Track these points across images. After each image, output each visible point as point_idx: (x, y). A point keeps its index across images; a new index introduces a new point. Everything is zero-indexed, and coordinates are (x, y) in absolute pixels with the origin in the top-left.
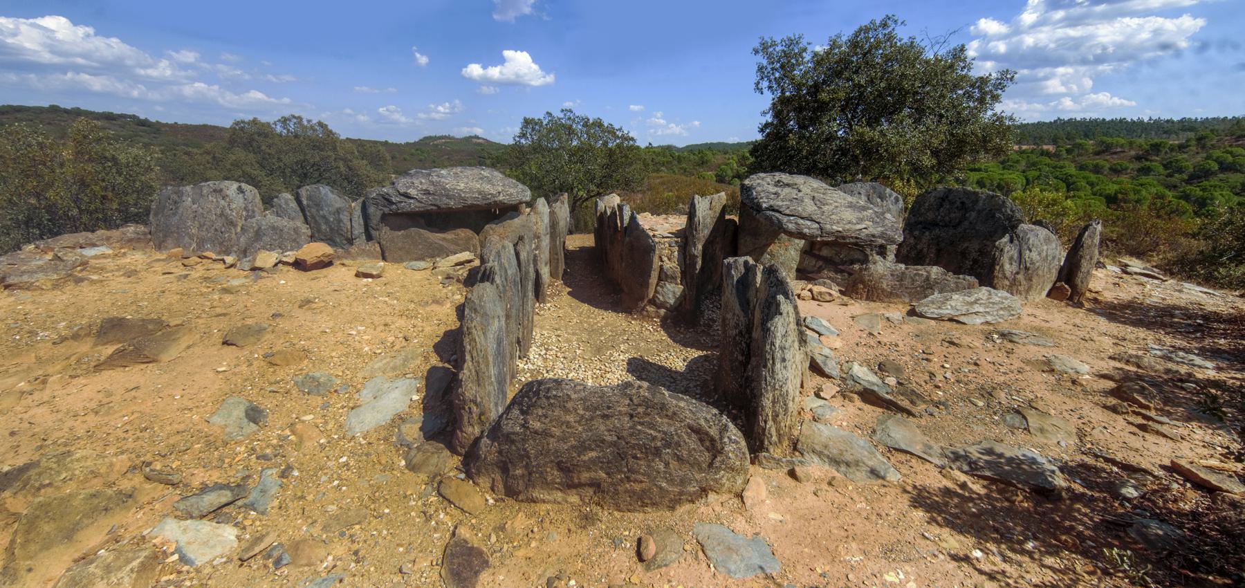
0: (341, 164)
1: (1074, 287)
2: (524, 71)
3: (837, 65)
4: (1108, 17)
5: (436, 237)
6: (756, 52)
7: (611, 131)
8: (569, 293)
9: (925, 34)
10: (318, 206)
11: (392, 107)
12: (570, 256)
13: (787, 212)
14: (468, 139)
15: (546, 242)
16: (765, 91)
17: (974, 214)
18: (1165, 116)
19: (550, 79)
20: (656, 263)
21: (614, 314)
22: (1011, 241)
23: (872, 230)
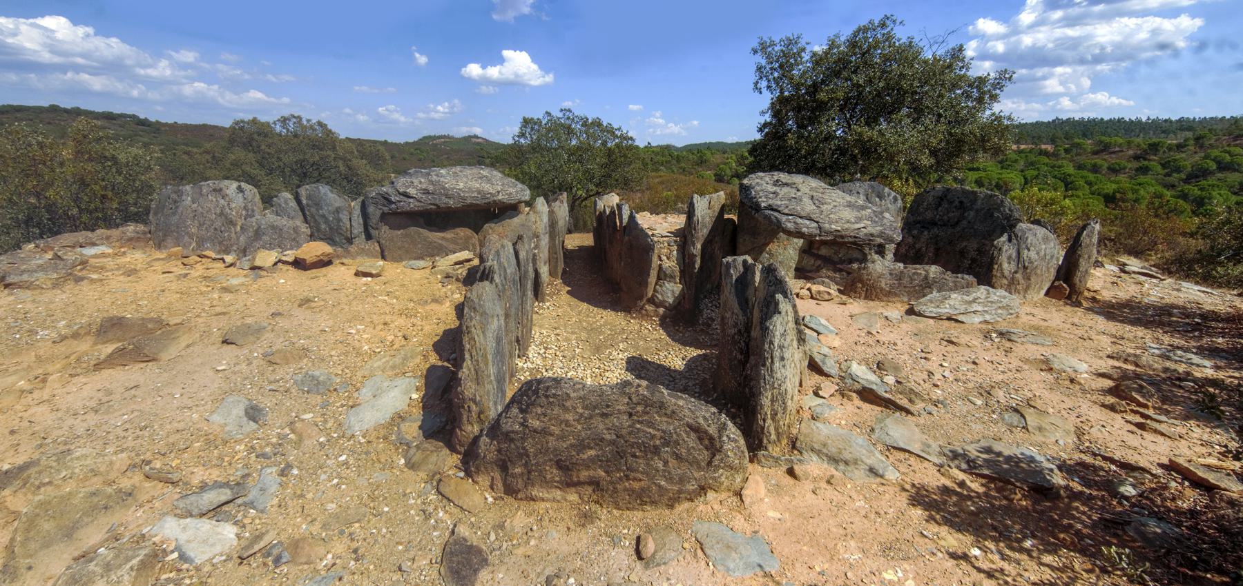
0: (340, 164)
1: (1072, 286)
2: (523, 70)
3: (836, 65)
4: (1106, 17)
5: (436, 236)
6: (755, 52)
7: (610, 131)
8: (568, 292)
9: (923, 34)
10: (317, 205)
11: (392, 107)
12: (569, 255)
13: (786, 211)
14: (467, 139)
15: (545, 241)
16: (764, 90)
17: (972, 213)
18: (1163, 116)
19: (549, 78)
20: (655, 262)
21: (613, 313)
22: (1010, 240)
23: (870, 230)
